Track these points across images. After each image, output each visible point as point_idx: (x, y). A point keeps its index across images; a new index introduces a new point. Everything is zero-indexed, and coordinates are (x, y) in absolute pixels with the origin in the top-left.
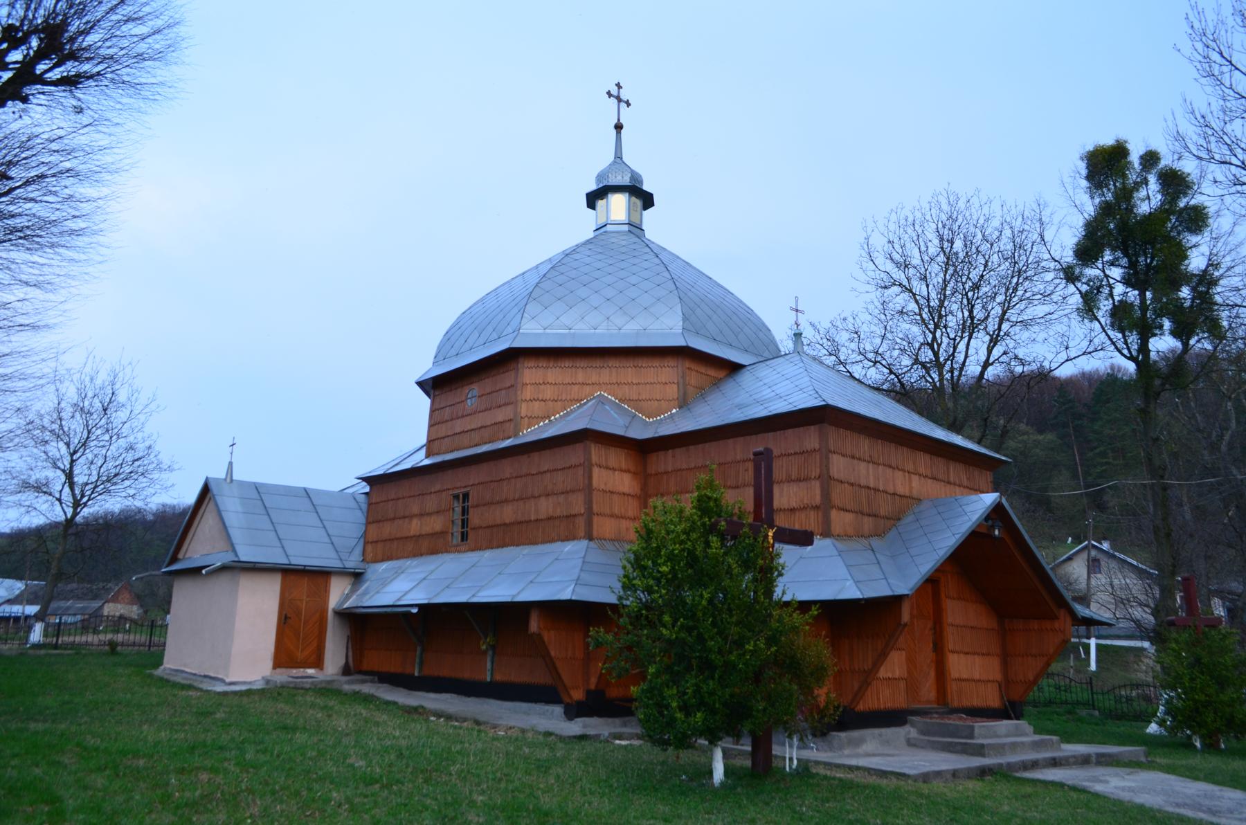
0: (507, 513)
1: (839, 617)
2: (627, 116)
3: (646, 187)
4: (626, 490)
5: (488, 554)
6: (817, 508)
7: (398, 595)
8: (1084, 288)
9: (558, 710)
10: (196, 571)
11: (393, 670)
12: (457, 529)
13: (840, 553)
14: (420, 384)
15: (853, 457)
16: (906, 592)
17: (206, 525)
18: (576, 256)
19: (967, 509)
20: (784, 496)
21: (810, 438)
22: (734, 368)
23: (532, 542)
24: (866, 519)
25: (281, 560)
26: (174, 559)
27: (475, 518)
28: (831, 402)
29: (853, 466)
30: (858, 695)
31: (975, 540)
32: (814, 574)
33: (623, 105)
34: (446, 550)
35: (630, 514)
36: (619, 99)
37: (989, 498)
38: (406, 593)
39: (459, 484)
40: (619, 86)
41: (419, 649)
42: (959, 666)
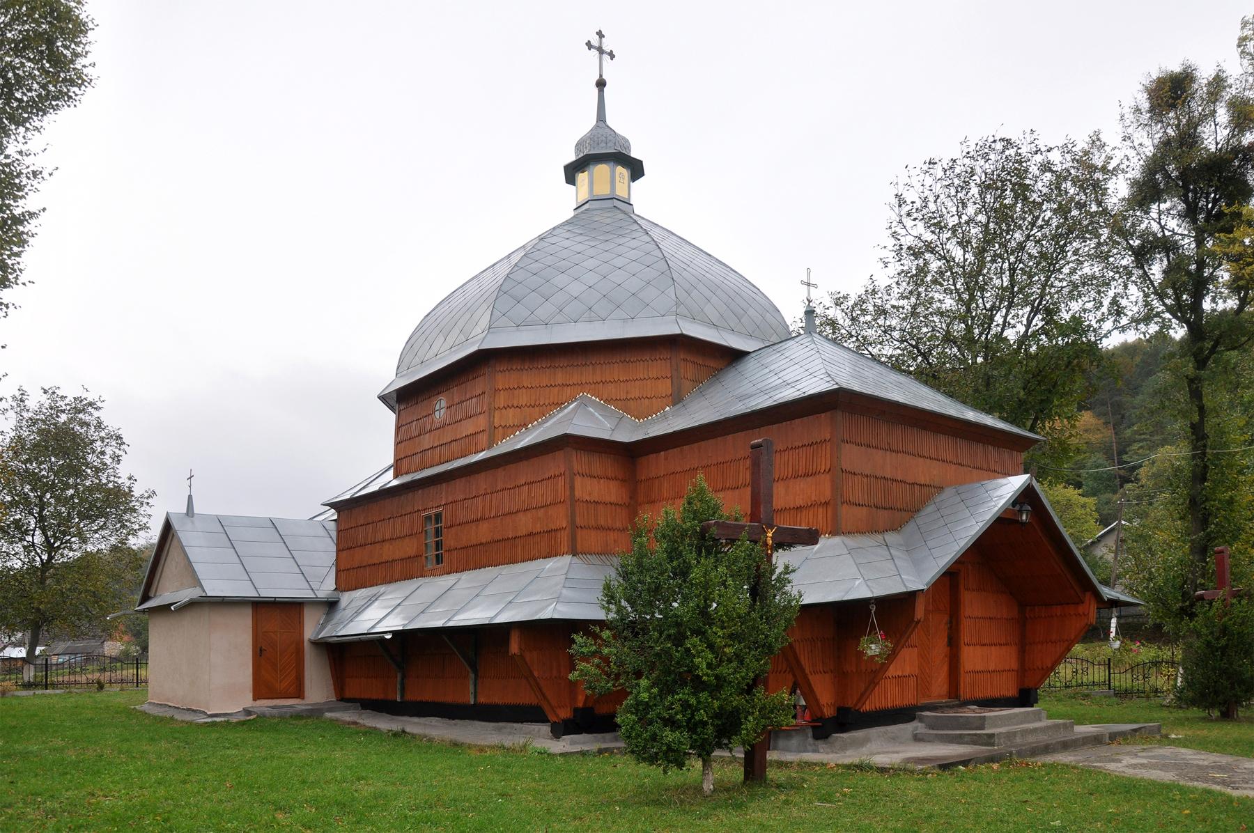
0: (483, 533)
1: (845, 619)
2: (611, 71)
3: (634, 154)
4: (613, 499)
5: (465, 576)
6: (827, 503)
7: (461, 585)
8: (1136, 243)
9: (545, 729)
10: (165, 609)
11: (374, 697)
12: (432, 553)
13: (850, 551)
14: (383, 398)
15: (869, 446)
16: (922, 587)
17: (171, 567)
18: (553, 240)
19: (999, 493)
20: (782, 496)
21: (820, 428)
22: (734, 357)
23: (512, 561)
24: (881, 512)
25: (249, 592)
26: (146, 598)
27: (449, 540)
28: (845, 385)
29: (866, 459)
30: (863, 696)
31: (1003, 524)
32: (826, 573)
33: (606, 57)
34: (421, 574)
35: (618, 525)
36: (601, 51)
37: (1017, 482)
38: (381, 620)
39: (430, 505)
40: (600, 34)
41: (399, 675)
42: (972, 658)
